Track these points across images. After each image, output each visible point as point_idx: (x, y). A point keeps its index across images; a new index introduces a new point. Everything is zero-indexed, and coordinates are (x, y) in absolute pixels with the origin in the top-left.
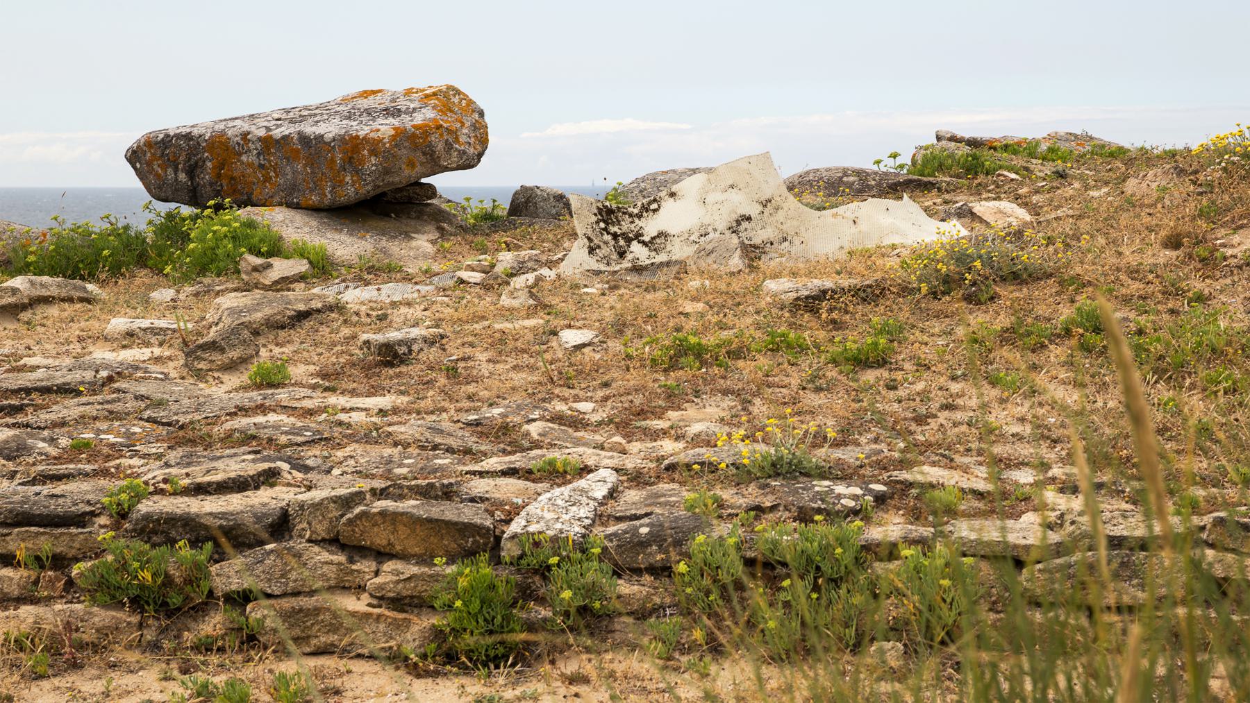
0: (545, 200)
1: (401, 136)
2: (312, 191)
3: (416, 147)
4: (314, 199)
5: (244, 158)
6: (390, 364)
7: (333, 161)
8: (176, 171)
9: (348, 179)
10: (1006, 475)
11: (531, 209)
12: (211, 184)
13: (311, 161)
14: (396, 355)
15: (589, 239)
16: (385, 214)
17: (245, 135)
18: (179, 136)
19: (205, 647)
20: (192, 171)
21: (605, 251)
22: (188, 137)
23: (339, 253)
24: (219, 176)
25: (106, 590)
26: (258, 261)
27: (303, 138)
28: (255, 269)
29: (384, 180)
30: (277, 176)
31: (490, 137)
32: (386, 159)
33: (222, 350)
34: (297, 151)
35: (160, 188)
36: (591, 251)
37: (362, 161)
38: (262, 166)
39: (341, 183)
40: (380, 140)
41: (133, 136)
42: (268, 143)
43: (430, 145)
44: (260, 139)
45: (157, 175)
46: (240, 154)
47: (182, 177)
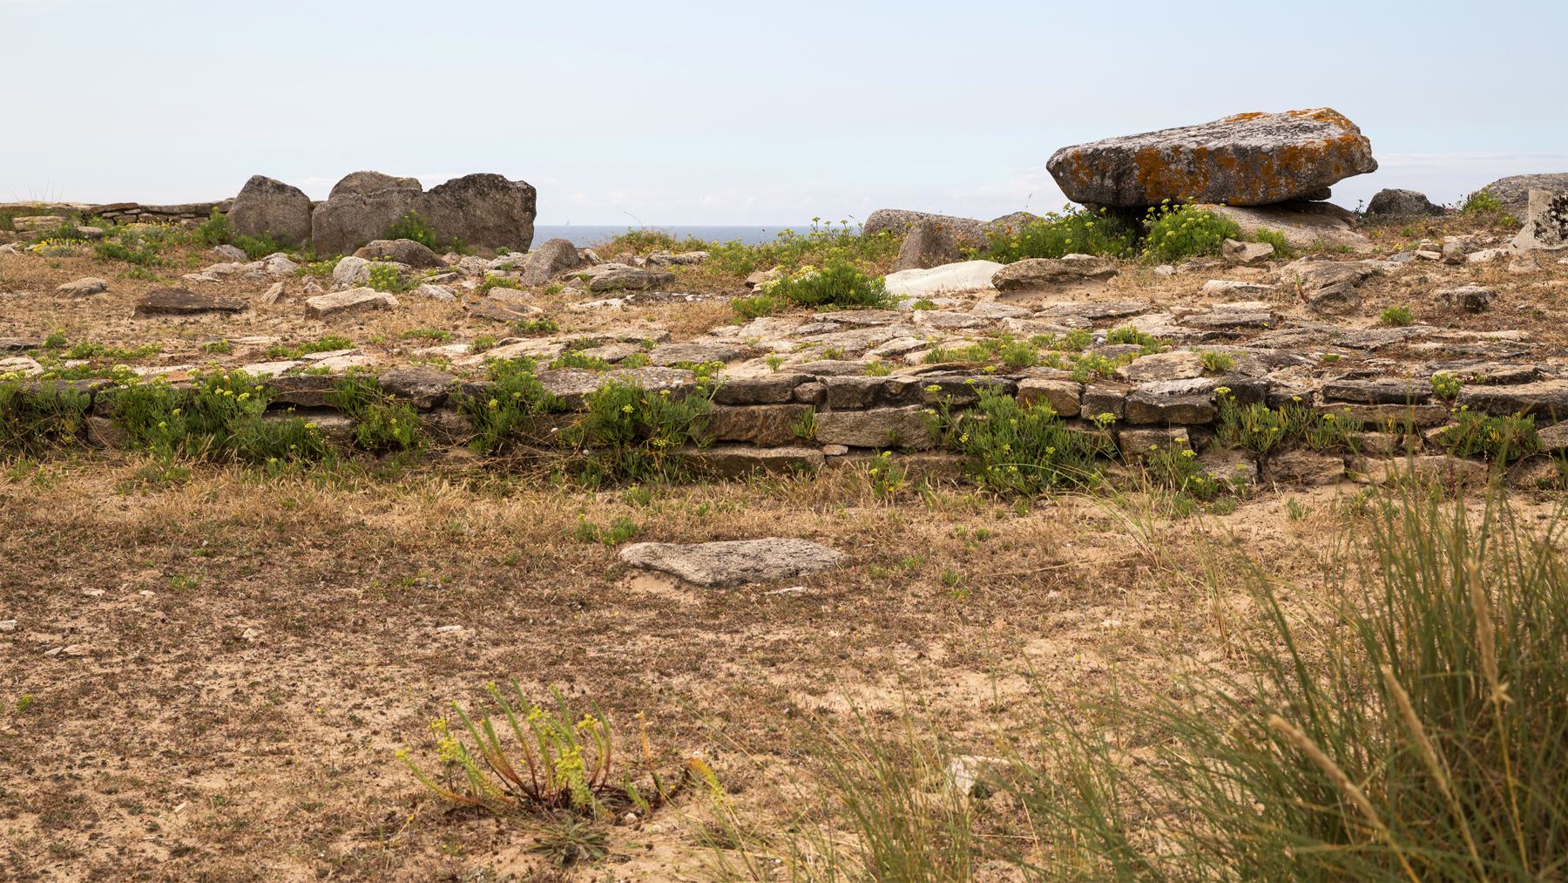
0: (1407, 200)
1: (1331, 145)
2: (1242, 192)
3: (1341, 156)
4: (1245, 198)
5: (1173, 167)
6: (1477, 312)
7: (1270, 167)
8: (1103, 177)
9: (1282, 181)
10: (1174, 796)
11: (1389, 209)
12: (1136, 188)
13: (1245, 167)
14: (1479, 304)
15: (1538, 225)
16: (1298, 211)
17: (1176, 149)
18: (1109, 150)
19: (1543, 485)
20: (1118, 179)
21: (1551, 233)
22: (1118, 150)
23: (1292, 238)
24: (1145, 181)
25: (1455, 445)
26: (1237, 244)
27: (1241, 151)
28: (1236, 250)
29: (1291, 179)
30: (1206, 180)
31: (367, 169)
32: (1321, 165)
33: (1344, 300)
34: (1232, 160)
35: (1082, 192)
36: (1537, 234)
37: (1299, 167)
38: (1190, 173)
39: (1276, 185)
40: (1317, 150)
41: (1048, 152)
42: (1200, 154)
43: (1352, 154)
44: (1192, 151)
45: (1082, 182)
46: (1168, 163)
47: (1109, 182)
